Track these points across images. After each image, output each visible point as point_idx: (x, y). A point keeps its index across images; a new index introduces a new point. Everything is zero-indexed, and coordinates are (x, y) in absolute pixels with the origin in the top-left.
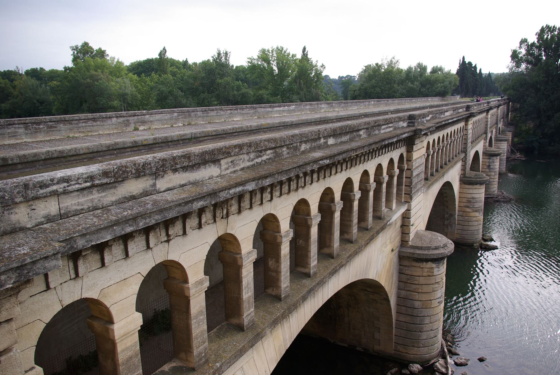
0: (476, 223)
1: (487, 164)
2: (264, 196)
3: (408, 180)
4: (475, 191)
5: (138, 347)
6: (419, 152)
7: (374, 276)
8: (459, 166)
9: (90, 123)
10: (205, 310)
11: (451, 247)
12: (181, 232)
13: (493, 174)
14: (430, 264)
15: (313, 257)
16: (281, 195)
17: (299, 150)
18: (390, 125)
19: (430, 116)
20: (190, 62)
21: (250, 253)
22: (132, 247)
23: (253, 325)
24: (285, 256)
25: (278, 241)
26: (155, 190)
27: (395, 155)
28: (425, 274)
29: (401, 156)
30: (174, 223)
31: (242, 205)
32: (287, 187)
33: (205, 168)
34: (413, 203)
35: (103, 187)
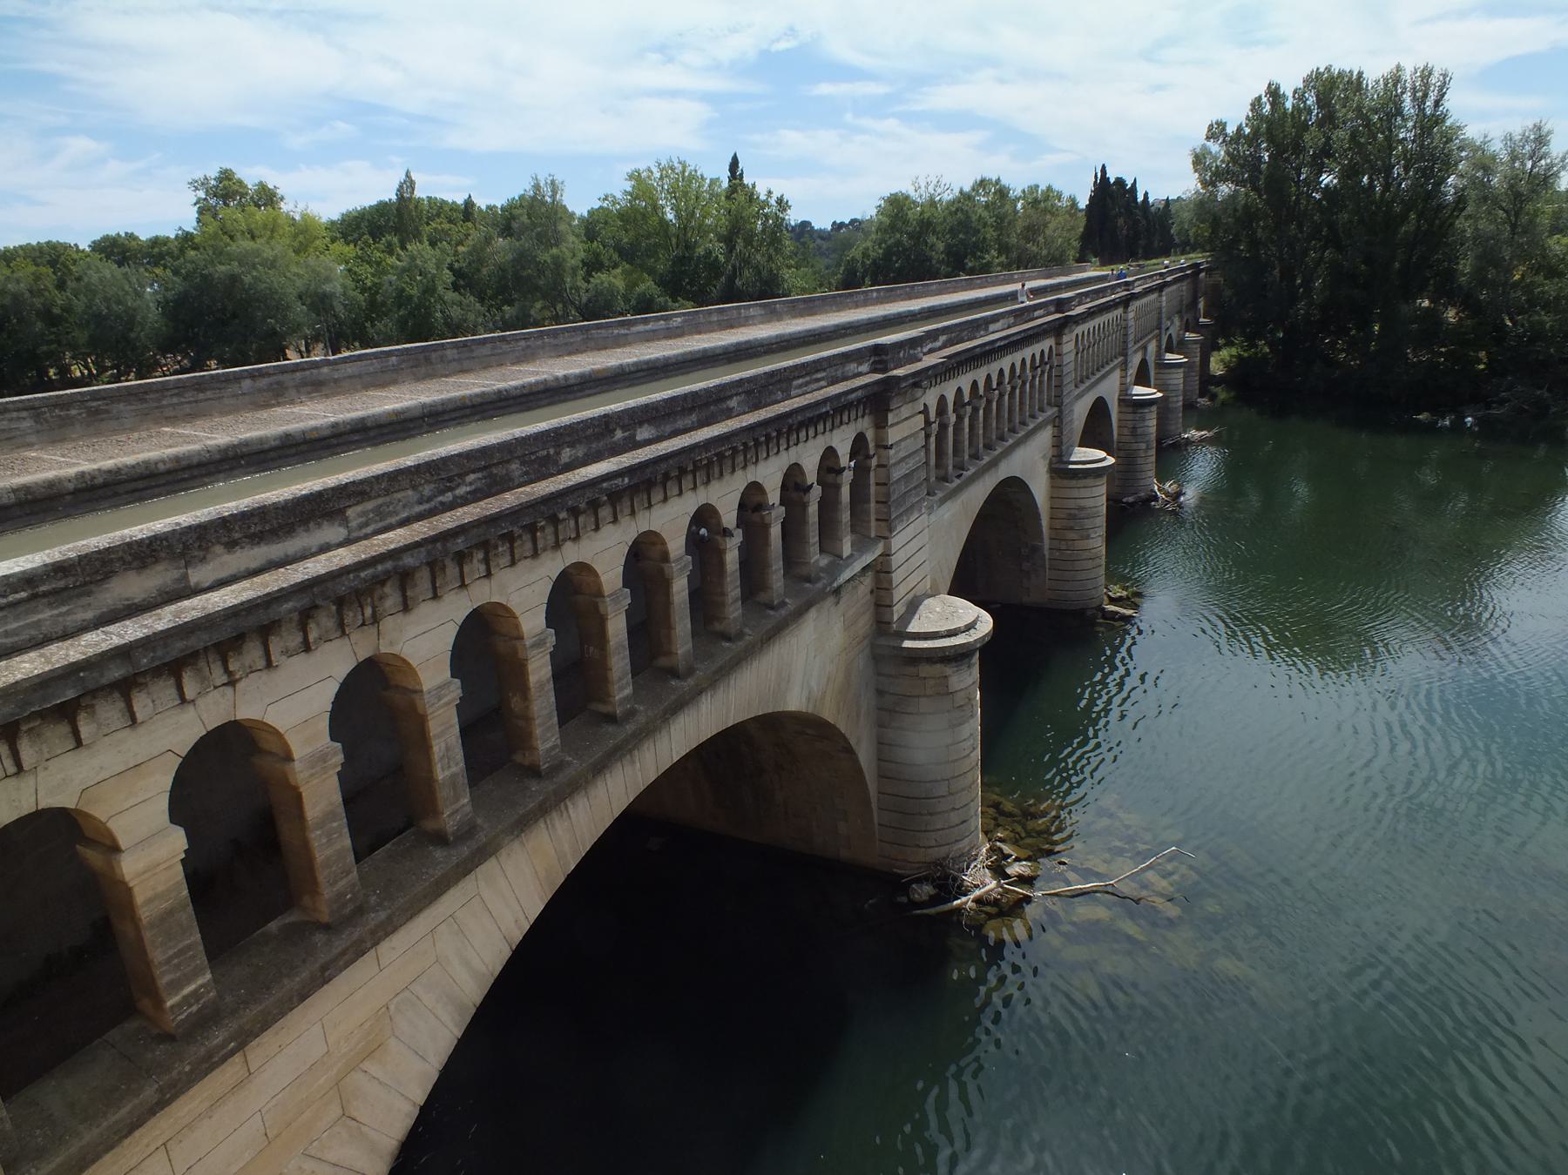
0: (1090, 564)
1: (1130, 424)
2: (466, 569)
3: (883, 489)
4: (1084, 493)
5: (185, 892)
6: (905, 428)
7: (75, 800)
8: (1045, 437)
9: (190, 396)
10: (341, 810)
11: (986, 623)
12: (261, 663)
13: (1143, 446)
14: (938, 669)
15: (620, 679)
16: (513, 563)
17: (556, 462)
18: (819, 376)
19: (943, 338)
20: (481, 202)
21: (441, 687)
22: (141, 703)
23: (468, 831)
24: (541, 685)
25: (521, 655)
26: (188, 587)
27: (842, 440)
28: (929, 692)
29: (860, 440)
30: (240, 647)
31: (409, 593)
32: (529, 545)
33: (307, 530)
34: (896, 542)
35: (57, 597)
